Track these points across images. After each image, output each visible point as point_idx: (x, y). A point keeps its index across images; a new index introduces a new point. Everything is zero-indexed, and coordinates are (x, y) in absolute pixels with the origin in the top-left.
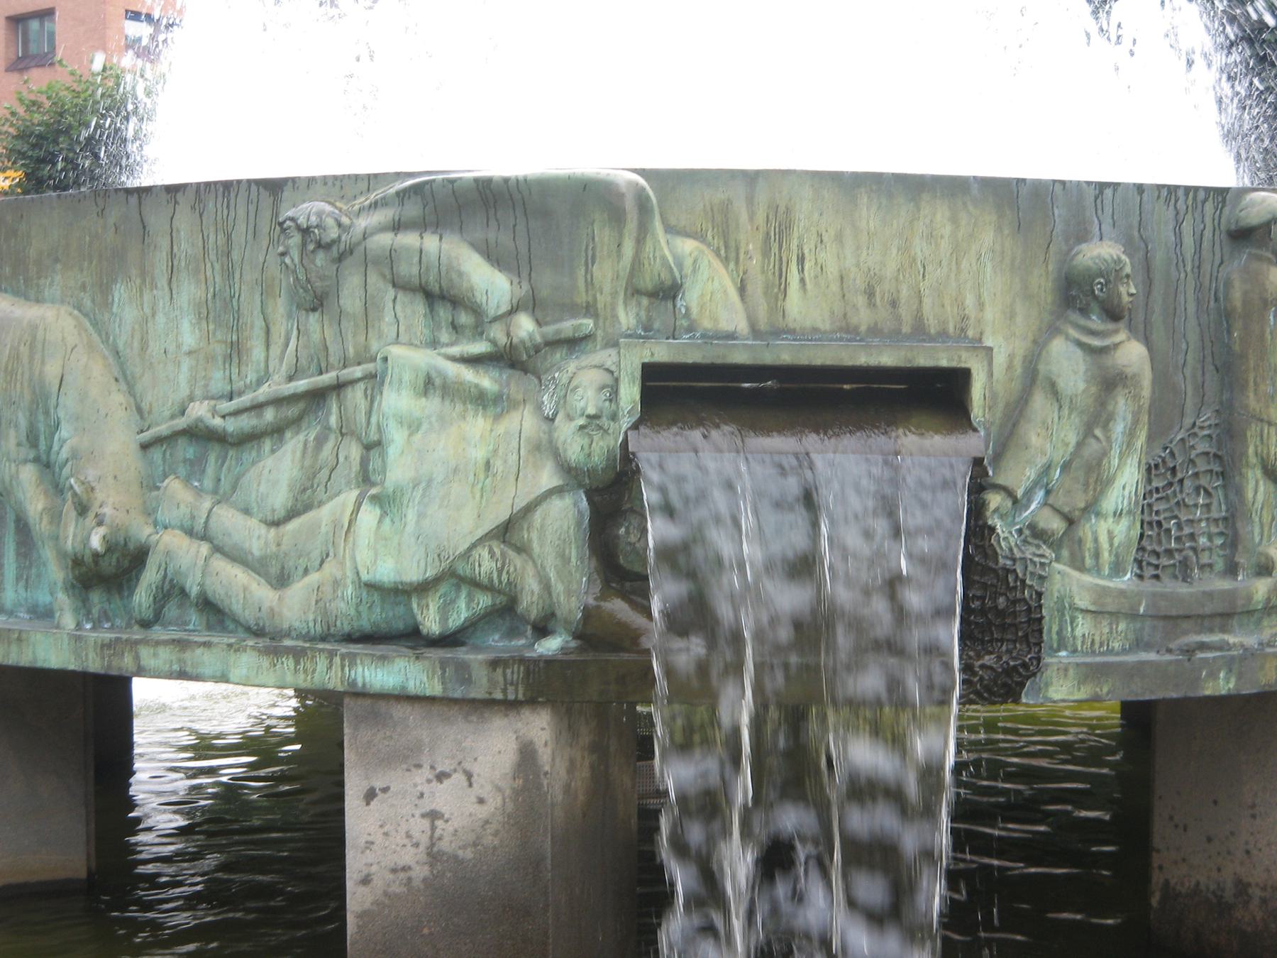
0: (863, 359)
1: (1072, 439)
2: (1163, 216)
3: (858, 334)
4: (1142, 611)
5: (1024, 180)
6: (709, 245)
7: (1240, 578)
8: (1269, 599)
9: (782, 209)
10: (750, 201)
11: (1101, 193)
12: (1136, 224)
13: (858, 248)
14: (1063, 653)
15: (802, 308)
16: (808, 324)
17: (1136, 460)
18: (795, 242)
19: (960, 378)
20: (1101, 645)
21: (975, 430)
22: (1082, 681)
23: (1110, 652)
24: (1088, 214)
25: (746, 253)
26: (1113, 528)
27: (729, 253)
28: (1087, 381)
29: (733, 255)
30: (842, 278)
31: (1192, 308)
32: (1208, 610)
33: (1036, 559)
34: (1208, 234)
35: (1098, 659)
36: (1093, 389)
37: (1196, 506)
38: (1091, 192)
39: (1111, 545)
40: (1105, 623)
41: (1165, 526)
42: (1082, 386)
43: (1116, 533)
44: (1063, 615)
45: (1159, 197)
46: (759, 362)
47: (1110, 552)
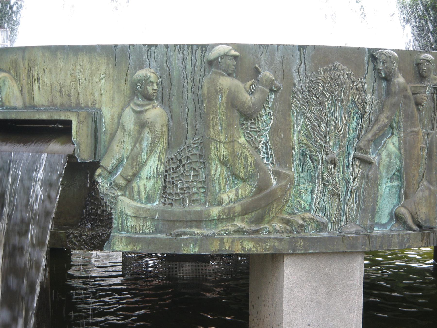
0: (37, 117)
1: (130, 148)
2: (177, 57)
3: (57, 107)
4: (156, 217)
5: (117, 46)
6: (12, 75)
7: (207, 206)
8: (219, 216)
9: (32, 61)
10: (23, 58)
11: (150, 49)
12: (165, 61)
13: (57, 74)
14: (124, 233)
15: (40, 98)
16: (41, 103)
17: (157, 156)
18: (37, 73)
19: (68, 123)
20: (140, 230)
21: (73, 144)
22: (128, 244)
23: (144, 233)
24: (144, 58)
25: (22, 77)
26: (146, 183)
27: (17, 78)
28: (134, 125)
29: (19, 78)
30: (51, 86)
31: (190, 95)
32: (188, 218)
33: (111, 195)
34: (198, 63)
35: (137, 236)
36: (137, 128)
37: (190, 175)
38: (146, 48)
39: (145, 190)
40: (141, 221)
41: (176, 183)
42: (132, 126)
43: (148, 185)
44: (123, 217)
45: (175, 49)
46: (6, 118)
47: (145, 193)
